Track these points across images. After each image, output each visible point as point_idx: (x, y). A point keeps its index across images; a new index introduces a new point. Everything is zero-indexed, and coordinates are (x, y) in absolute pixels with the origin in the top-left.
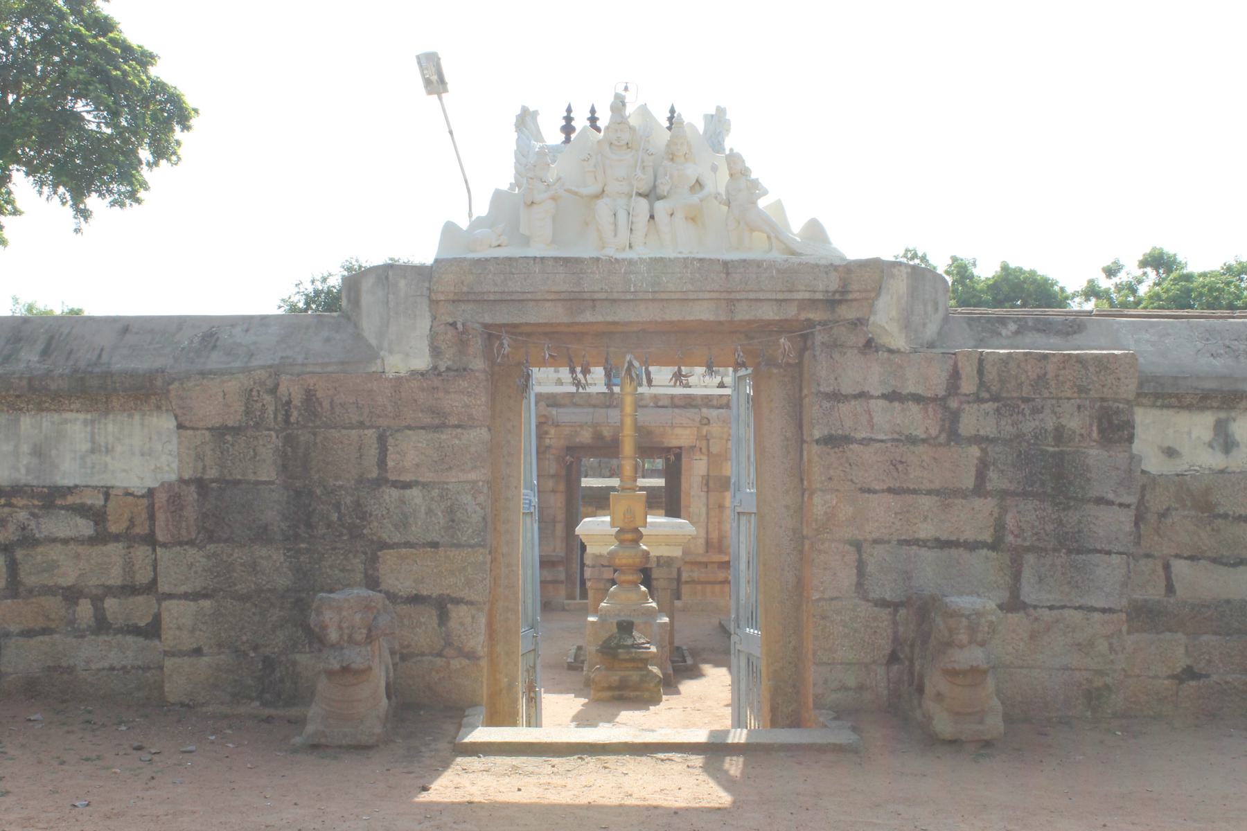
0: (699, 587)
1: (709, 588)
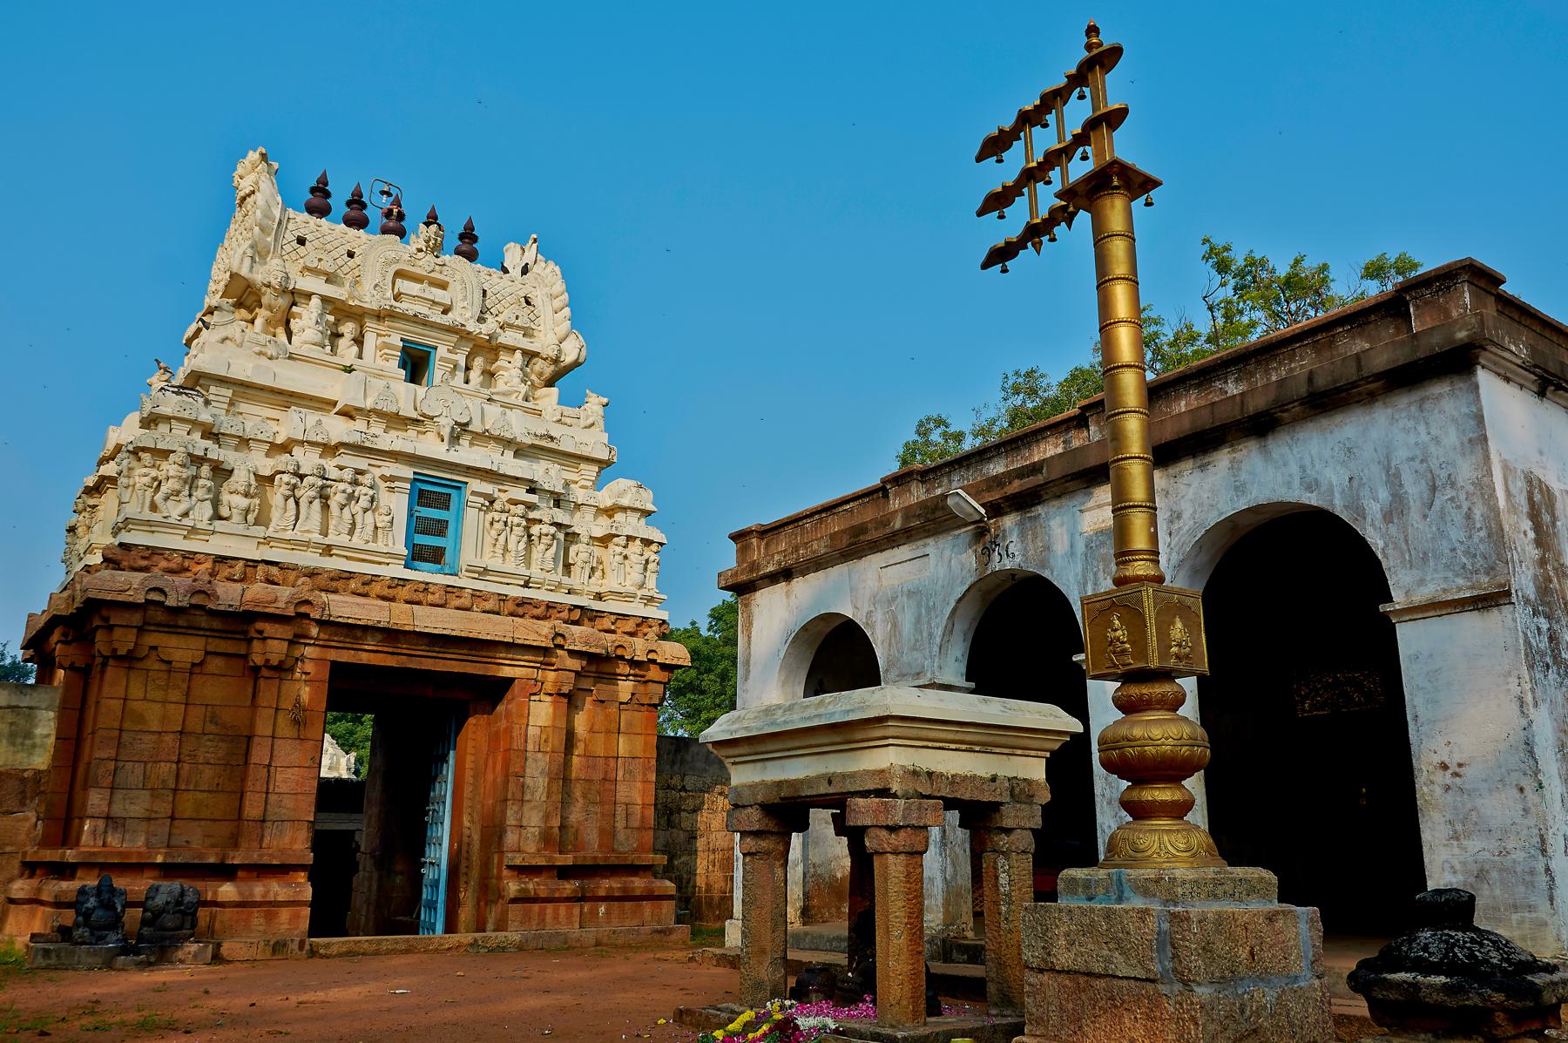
0: (536, 907)
1: (550, 908)
